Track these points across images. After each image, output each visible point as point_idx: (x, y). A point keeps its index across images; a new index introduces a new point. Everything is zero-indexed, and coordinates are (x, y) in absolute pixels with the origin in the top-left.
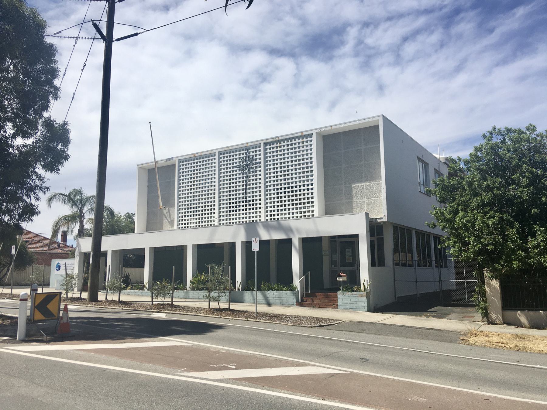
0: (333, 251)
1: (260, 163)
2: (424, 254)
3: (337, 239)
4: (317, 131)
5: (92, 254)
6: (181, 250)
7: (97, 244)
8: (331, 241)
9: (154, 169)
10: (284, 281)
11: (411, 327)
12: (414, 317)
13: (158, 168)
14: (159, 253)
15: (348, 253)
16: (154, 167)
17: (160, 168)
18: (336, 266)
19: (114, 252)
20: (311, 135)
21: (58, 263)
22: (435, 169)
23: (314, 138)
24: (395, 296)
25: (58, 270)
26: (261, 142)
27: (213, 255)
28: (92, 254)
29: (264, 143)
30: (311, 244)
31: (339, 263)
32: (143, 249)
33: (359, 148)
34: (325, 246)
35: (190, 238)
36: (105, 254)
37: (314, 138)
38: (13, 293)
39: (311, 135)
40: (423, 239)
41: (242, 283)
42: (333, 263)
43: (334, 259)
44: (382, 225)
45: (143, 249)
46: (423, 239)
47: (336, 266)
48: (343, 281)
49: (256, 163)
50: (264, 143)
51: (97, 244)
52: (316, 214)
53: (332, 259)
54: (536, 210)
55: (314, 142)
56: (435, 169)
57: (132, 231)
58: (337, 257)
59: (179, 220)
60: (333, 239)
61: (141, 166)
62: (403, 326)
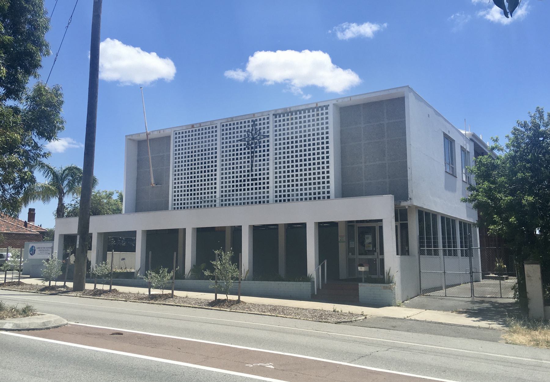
0: (350, 237)
1: (268, 136)
2: (449, 241)
3: (355, 224)
4: (335, 102)
5: (78, 237)
6: (297, 231)
7: (84, 226)
8: (349, 225)
9: (145, 141)
10: (298, 270)
11: (445, 324)
12: (445, 313)
13: (150, 140)
14: (263, 234)
15: (368, 239)
16: (145, 138)
17: (152, 140)
18: (353, 254)
19: (100, 234)
20: (327, 107)
21: (33, 247)
22: (461, 147)
23: (331, 110)
24: (420, 289)
25: (32, 255)
26: (269, 113)
27: (212, 240)
28: (78, 237)
29: (273, 115)
30: (327, 230)
31: (357, 251)
32: (134, 233)
33: (382, 122)
34: (342, 231)
35: (187, 221)
36: (91, 236)
37: (331, 110)
38: (174, 294)
39: (327, 107)
40: (448, 224)
41: (192, 270)
42: (350, 250)
43: (352, 246)
44: (407, 209)
45: (134, 233)
46: (448, 224)
47: (353, 254)
48: (365, 271)
49: (264, 137)
50: (273, 115)
51: (84, 226)
52: (332, 194)
53: (349, 246)
54: (530, 199)
55: (331, 116)
56: (461, 147)
57: (166, 208)
58: (355, 244)
59: (175, 200)
60: (350, 224)
61: (130, 137)
62: (436, 323)
